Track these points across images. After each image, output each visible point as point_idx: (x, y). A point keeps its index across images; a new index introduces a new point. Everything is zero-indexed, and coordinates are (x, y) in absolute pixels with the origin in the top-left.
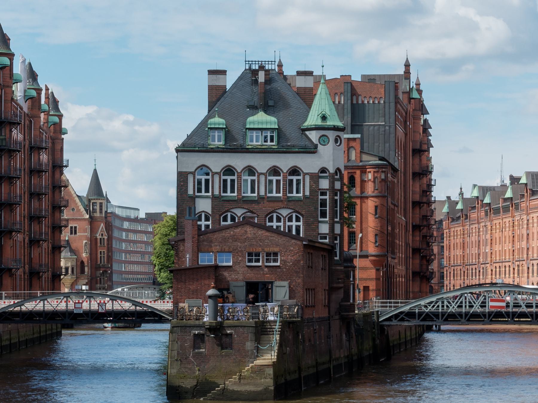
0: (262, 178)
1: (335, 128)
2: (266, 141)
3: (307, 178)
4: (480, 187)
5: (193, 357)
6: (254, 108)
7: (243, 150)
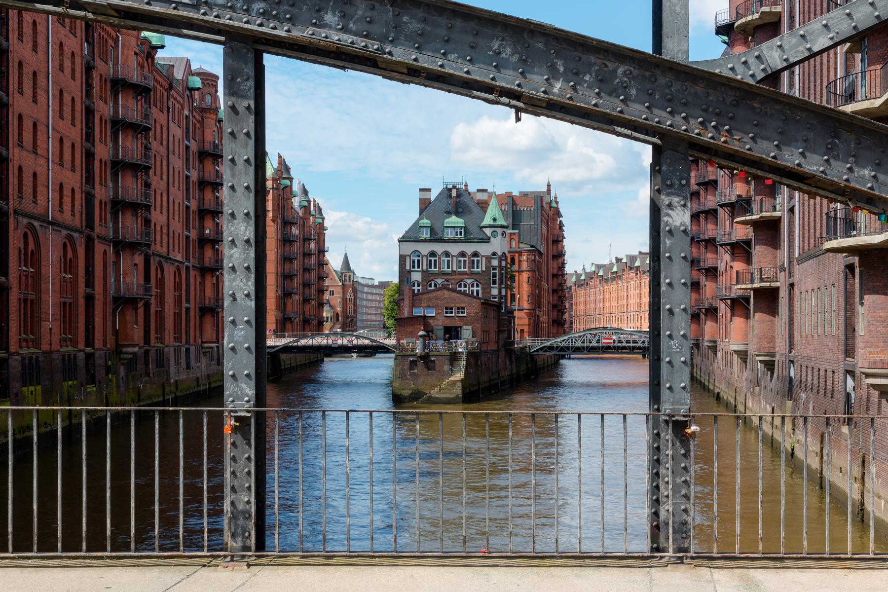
1: (502, 227)
3: (484, 259)
5: (410, 375)
6: (449, 213)
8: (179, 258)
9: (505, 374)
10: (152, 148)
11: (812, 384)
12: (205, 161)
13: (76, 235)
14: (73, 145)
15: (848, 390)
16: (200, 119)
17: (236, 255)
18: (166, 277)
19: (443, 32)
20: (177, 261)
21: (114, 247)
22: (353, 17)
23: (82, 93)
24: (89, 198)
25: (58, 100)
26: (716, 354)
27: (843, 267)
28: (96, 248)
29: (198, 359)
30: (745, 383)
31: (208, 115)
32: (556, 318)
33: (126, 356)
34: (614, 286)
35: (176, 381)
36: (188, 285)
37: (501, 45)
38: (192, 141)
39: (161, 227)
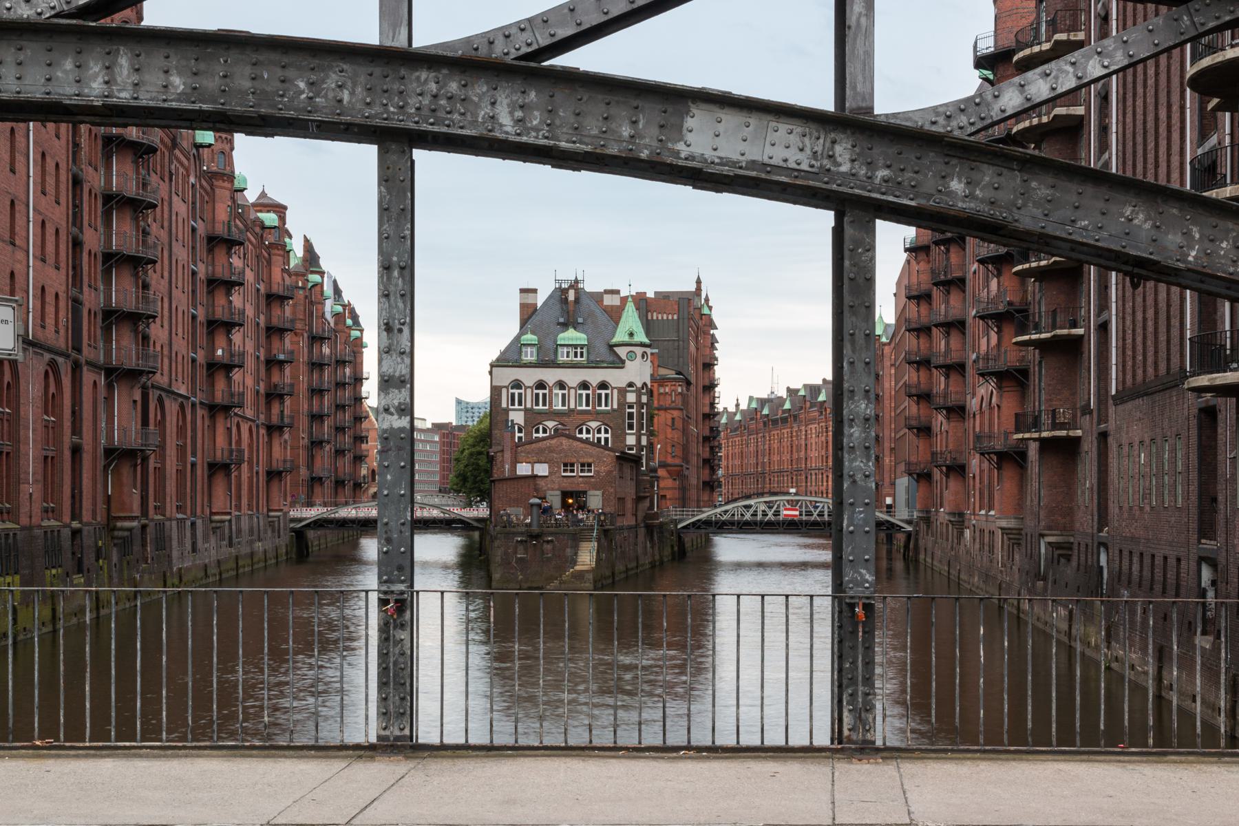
0: (572, 391)
1: (642, 345)
2: (576, 356)
3: (615, 392)
4: (758, 399)
5: (516, 563)
6: (565, 326)
7: (553, 364)
8: (183, 391)
9: (646, 561)
10: (151, 232)
11: (1141, 577)
12: (217, 250)
13: (60, 360)
14: (57, 231)
15: (1203, 585)
16: (208, 188)
17: (857, 434)
18: (168, 419)
19: (1074, 198)
20: (181, 396)
21: (107, 377)
22: (979, 184)
23: (68, 157)
24: (76, 303)
25: (39, 168)
26: (961, 534)
27: (1197, 411)
28: (84, 379)
29: (206, 539)
30: (1017, 576)
31: (220, 183)
32: (708, 479)
33: (120, 534)
34: (785, 431)
35: (180, 569)
36: (194, 430)
37: (1133, 211)
38: (200, 221)
39: (162, 347)
